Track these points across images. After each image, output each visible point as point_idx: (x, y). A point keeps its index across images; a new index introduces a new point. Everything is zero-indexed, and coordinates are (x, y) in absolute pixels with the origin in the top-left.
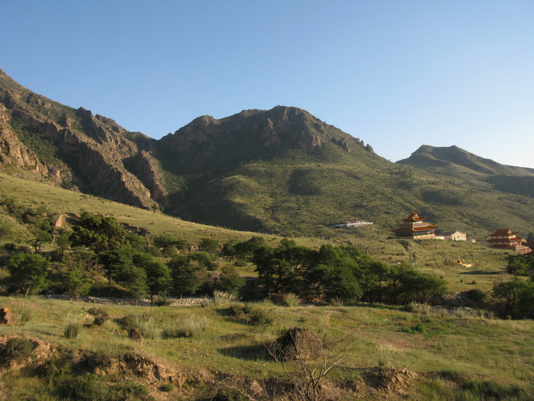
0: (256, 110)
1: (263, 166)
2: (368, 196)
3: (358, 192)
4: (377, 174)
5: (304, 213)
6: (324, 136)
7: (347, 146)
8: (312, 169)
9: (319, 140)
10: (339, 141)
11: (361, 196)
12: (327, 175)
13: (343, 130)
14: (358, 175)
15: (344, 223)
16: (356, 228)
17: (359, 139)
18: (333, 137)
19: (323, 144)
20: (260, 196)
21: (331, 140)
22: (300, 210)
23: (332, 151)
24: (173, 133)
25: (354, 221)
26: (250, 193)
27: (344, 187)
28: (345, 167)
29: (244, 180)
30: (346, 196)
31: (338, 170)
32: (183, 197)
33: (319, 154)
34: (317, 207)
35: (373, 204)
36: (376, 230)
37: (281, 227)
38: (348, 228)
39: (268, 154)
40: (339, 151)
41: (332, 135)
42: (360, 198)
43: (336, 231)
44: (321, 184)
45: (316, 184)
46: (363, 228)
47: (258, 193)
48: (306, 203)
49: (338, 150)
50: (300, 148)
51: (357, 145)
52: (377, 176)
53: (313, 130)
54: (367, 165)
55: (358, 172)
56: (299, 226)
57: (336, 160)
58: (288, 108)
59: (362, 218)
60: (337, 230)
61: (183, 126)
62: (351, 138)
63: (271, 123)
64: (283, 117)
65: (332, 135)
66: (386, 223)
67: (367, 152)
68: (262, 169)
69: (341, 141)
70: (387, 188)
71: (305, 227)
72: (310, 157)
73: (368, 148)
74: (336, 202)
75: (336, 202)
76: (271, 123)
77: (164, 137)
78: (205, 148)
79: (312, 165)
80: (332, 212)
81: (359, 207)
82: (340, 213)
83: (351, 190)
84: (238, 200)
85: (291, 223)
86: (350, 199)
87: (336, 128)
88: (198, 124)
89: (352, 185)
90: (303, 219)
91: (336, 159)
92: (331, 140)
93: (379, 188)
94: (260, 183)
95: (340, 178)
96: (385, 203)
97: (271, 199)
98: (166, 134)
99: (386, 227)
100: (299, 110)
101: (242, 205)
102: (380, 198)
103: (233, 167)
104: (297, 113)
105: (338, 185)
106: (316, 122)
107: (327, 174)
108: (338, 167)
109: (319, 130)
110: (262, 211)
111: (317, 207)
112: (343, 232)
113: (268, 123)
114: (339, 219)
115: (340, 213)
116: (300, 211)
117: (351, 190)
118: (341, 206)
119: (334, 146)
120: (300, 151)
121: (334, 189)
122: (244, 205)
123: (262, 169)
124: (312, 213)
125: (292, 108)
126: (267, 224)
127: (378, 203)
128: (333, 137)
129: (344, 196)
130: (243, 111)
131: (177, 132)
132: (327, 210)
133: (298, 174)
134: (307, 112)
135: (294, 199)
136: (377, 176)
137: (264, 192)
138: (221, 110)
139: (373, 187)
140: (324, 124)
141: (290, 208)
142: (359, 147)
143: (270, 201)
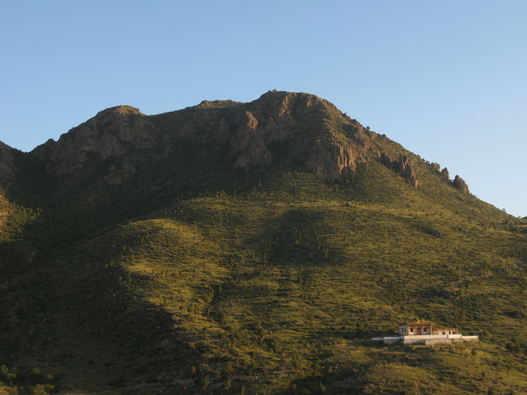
0: (230, 102)
1: (223, 204)
2: (460, 272)
3: (437, 261)
4: (480, 228)
5: (293, 304)
6: (365, 150)
7: (413, 174)
8: (331, 212)
9: (351, 158)
10: (395, 163)
11: (440, 270)
12: (364, 224)
13: (405, 147)
14: (437, 227)
15: (398, 335)
16: (430, 350)
17: (438, 166)
18: (383, 155)
19: (360, 166)
20: (198, 261)
21: (378, 160)
22: (284, 295)
23: (380, 181)
24: (56, 139)
25: (427, 330)
26: (174, 253)
27: (402, 250)
28: (406, 212)
29: (174, 227)
30: (407, 270)
31: (391, 216)
32: (30, 260)
33: (350, 185)
34: (330, 290)
35: (474, 290)
36: (489, 357)
37: (219, 336)
38: (408, 348)
39: (243, 181)
40: (395, 182)
41: (380, 149)
42: (440, 276)
43: (371, 354)
44: (347, 241)
45: (335, 240)
46: (450, 349)
47: (195, 254)
48: (305, 279)
49: (392, 180)
50: (310, 171)
51: (433, 176)
52: (481, 232)
53: (341, 136)
54: (457, 213)
55: (436, 221)
56: (272, 335)
57: (387, 198)
58: (293, 94)
59: (445, 322)
60: (374, 350)
61: (76, 125)
62: (421, 162)
63: (253, 122)
64: (279, 111)
65: (380, 149)
66: (513, 340)
67: (455, 191)
68: (220, 208)
69: (399, 163)
70: (505, 257)
71: (287, 339)
72: (330, 190)
73: (458, 184)
74: (381, 280)
75: (381, 280)
76: (253, 122)
77: (38, 147)
78: (112, 168)
79: (334, 204)
80: (367, 305)
81: (440, 295)
82: (390, 307)
83: (419, 257)
84: (141, 267)
85: (251, 327)
86: (416, 277)
87: (391, 142)
88: (111, 123)
89: (422, 247)
90: (286, 316)
91: (387, 195)
92: (378, 160)
93: (487, 257)
94: (207, 235)
95: (392, 231)
96: (506, 290)
97: (222, 269)
98: (43, 141)
99: (517, 350)
100: (314, 98)
101: (142, 280)
102: (490, 278)
103: (163, 202)
104: (309, 104)
105: (387, 245)
106: (348, 123)
107: (365, 221)
108: (392, 211)
109: (354, 138)
110: (187, 293)
111: (330, 290)
112: (391, 359)
113: (247, 119)
114: (384, 323)
115: (387, 307)
116: (283, 299)
117: (419, 257)
118: (391, 291)
119: (384, 170)
120: (309, 176)
121: (377, 253)
122: (148, 278)
123: (220, 208)
124: (313, 303)
125: (299, 95)
126: (186, 325)
127: (487, 289)
128: (383, 155)
129: (400, 269)
130: (203, 102)
131: (63, 136)
132: (355, 299)
133: (300, 218)
134: (331, 105)
135: (276, 271)
136: (481, 232)
137: (209, 254)
138: (158, 97)
139: (471, 254)
140: (367, 131)
141: (263, 291)
142: (439, 180)
143: (216, 271)
